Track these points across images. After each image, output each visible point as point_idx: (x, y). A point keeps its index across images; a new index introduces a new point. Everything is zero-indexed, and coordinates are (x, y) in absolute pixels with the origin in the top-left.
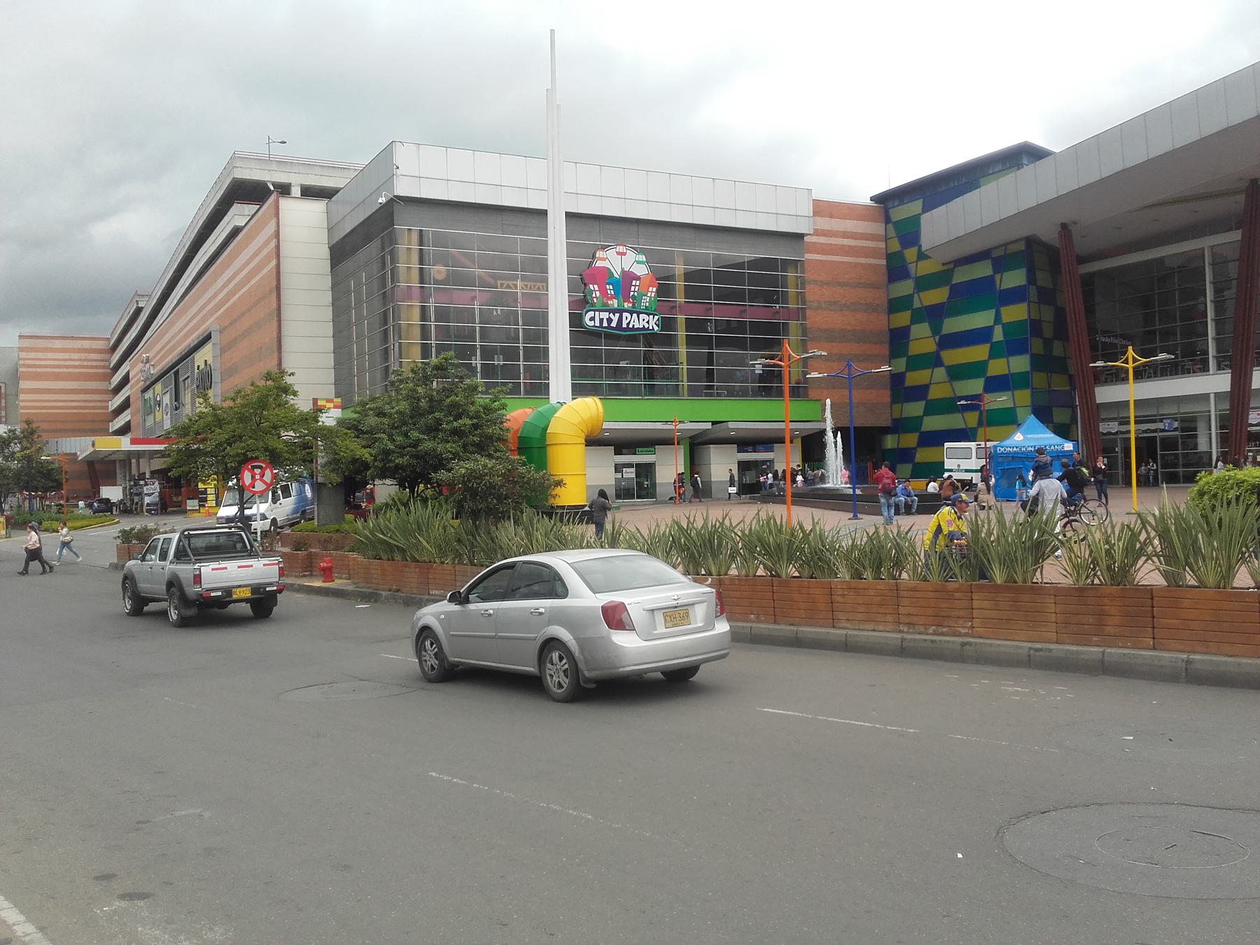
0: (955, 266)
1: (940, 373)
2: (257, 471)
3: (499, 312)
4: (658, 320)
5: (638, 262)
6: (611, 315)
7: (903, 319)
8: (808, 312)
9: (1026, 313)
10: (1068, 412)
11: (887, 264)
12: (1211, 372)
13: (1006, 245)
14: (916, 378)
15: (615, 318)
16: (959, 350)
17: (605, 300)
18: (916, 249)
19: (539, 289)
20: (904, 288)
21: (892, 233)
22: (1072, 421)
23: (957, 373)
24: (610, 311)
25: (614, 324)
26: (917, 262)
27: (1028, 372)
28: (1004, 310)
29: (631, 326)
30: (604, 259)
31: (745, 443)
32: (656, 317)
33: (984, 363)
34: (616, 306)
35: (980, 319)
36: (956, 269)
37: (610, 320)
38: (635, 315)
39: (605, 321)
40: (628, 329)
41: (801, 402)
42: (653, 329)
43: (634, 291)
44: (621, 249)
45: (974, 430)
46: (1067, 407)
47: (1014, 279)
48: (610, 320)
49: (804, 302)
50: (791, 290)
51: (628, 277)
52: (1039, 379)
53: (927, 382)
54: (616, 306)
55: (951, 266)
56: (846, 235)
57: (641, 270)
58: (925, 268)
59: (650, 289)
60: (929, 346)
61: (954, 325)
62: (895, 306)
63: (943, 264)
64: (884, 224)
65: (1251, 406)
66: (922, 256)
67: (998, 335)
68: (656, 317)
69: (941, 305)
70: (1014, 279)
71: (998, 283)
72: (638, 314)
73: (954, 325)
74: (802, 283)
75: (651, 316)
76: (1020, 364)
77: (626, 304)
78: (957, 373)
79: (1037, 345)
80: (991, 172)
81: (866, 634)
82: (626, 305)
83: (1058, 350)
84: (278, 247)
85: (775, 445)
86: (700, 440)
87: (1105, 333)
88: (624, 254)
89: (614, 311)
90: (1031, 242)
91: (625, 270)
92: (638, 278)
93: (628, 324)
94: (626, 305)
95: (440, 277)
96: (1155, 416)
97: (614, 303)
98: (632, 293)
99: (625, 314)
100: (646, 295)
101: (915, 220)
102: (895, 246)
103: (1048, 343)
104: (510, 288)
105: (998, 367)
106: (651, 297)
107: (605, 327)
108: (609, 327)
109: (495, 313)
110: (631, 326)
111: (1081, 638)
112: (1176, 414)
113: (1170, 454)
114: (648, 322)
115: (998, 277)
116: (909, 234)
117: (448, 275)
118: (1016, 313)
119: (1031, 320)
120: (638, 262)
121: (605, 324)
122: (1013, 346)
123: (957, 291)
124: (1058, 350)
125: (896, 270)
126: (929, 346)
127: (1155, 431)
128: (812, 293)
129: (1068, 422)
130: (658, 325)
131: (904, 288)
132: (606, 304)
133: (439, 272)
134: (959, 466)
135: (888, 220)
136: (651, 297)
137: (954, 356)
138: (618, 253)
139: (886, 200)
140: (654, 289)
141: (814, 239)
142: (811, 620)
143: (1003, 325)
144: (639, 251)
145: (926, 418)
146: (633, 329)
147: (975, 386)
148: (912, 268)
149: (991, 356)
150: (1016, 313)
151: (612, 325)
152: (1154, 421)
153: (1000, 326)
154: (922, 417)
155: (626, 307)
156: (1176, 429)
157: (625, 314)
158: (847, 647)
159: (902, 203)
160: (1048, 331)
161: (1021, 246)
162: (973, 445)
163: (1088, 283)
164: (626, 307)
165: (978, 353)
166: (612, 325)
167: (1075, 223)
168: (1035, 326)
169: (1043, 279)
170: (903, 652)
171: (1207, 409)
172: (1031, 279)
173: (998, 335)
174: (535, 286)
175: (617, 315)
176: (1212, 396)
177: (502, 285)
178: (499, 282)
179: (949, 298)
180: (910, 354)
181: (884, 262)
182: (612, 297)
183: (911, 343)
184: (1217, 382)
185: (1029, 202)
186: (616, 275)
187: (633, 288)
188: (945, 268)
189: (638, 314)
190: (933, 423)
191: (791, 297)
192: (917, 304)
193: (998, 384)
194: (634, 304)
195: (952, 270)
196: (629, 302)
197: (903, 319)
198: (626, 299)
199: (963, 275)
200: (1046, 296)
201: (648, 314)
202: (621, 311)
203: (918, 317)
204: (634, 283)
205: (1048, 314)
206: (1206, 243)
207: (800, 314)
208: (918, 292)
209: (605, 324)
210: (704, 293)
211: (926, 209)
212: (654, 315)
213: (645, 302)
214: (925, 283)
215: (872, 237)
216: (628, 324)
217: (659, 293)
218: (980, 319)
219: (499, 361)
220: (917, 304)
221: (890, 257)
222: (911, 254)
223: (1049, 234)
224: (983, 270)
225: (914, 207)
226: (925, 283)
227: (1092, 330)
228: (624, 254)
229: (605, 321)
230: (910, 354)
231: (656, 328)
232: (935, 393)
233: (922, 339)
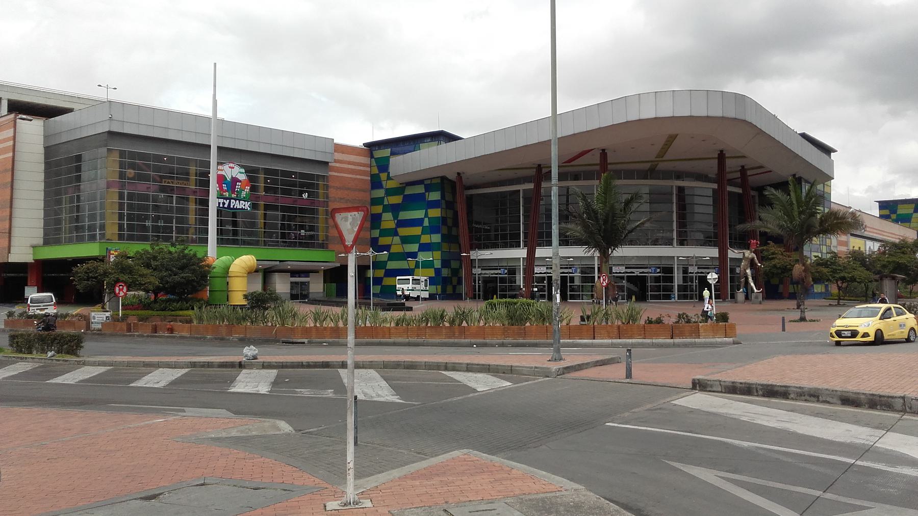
0: (407, 185)
1: (397, 239)
2: (121, 287)
3: (162, 196)
4: (250, 204)
5: (241, 173)
6: (225, 201)
7: (378, 209)
8: (330, 203)
9: (440, 213)
10: (458, 262)
11: (371, 180)
12: (521, 248)
13: (431, 179)
14: (383, 241)
15: (227, 202)
16: (405, 228)
17: (222, 193)
18: (386, 174)
19: (185, 185)
20: (380, 193)
21: (374, 164)
22: (460, 267)
23: (405, 240)
24: (224, 198)
25: (226, 206)
26: (386, 181)
27: (440, 243)
28: (429, 211)
29: (235, 207)
30: (222, 170)
31: (294, 273)
32: (249, 203)
33: (419, 237)
34: (227, 196)
35: (418, 214)
36: (407, 187)
37: (224, 204)
38: (237, 201)
39: (221, 204)
40: (233, 209)
41: (321, 252)
42: (247, 209)
43: (238, 188)
44: (231, 165)
45: (413, 270)
46: (458, 260)
47: (435, 196)
48: (224, 204)
49: (327, 197)
50: (321, 191)
51: (235, 180)
52: (445, 247)
53: (390, 243)
54: (227, 196)
55: (404, 185)
56: (349, 163)
57: (243, 177)
58: (391, 184)
59: (247, 188)
60: (392, 225)
61: (405, 215)
62: (375, 202)
63: (400, 184)
64: (370, 159)
65: (740, 179)
66: (389, 178)
67: (426, 223)
68: (249, 203)
69: (398, 205)
70: (435, 196)
71: (427, 198)
72: (239, 200)
73: (405, 215)
74: (327, 187)
75: (246, 202)
76: (436, 238)
77: (233, 195)
78: (405, 240)
79: (444, 230)
80: (425, 141)
81: (400, 340)
82: (233, 196)
83: (454, 232)
84: (14, 145)
85: (310, 274)
86: (272, 269)
87: (477, 223)
88: (233, 168)
89: (226, 199)
90: (443, 178)
91: (234, 176)
92: (240, 181)
93: (234, 206)
94: (233, 196)
95: (131, 176)
96: (497, 266)
97: (227, 194)
98: (236, 189)
99: (232, 200)
100: (244, 191)
101: (387, 158)
102: (375, 171)
103: (450, 228)
104: (170, 183)
105: (425, 239)
106: (246, 192)
107: (221, 207)
108: (223, 207)
109: (160, 197)
110: (235, 207)
111: (450, 338)
112: (506, 266)
113: (503, 286)
114: (244, 205)
115: (427, 194)
116: (383, 166)
117: (135, 175)
118: (435, 213)
119: (442, 217)
120: (241, 173)
121: (221, 206)
122: (433, 230)
123: (408, 199)
124: (454, 232)
125: (376, 183)
126: (392, 225)
127: (497, 274)
128: (332, 193)
129: (458, 268)
130: (250, 207)
131: (380, 193)
132: (222, 195)
133: (130, 173)
134: (408, 288)
135: (372, 157)
136: (246, 192)
137: (404, 231)
138: (230, 167)
139: (372, 147)
140: (249, 188)
141: (334, 164)
142: (383, 337)
143: (429, 218)
144: (242, 166)
145: (389, 262)
146: (237, 209)
147: (414, 248)
148: (384, 183)
149: (423, 233)
150: (435, 213)
151: (225, 206)
152: (497, 269)
153: (427, 219)
154: (387, 262)
155: (233, 196)
156: (506, 274)
157: (232, 200)
158: (394, 344)
159: (379, 149)
160: (450, 222)
161: (439, 181)
162: (410, 277)
163: (470, 198)
164: (233, 196)
165: (416, 231)
166: (225, 206)
167: (464, 173)
168: (444, 220)
169: (449, 197)
170: (409, 344)
171: (652, 196)
172: (443, 196)
173: (426, 223)
174: (178, 183)
175: (228, 201)
176: (522, 259)
177: (165, 182)
178: (164, 180)
179: (402, 202)
180: (381, 228)
181: (369, 178)
182: (226, 191)
183: (382, 222)
184: (521, 253)
185: (443, 161)
186: (228, 179)
187: (237, 187)
188: (401, 186)
189: (239, 200)
190: (392, 265)
191: (321, 195)
192: (386, 203)
193: (425, 247)
194: (237, 195)
195: (405, 187)
196: (235, 194)
197: (378, 209)
198: (233, 192)
199: (409, 191)
200: (450, 205)
201: (245, 201)
202: (230, 199)
203: (386, 209)
204: (238, 184)
205: (450, 214)
206: (521, 187)
207: (326, 204)
208: (386, 197)
209: (221, 206)
210: (275, 190)
211: (393, 154)
212: (248, 202)
213: (243, 194)
214: (390, 192)
215: (364, 165)
216: (234, 206)
217: (251, 190)
218: (418, 214)
219: (161, 224)
220: (386, 203)
221: (372, 176)
222: (383, 176)
223: (452, 176)
224: (420, 189)
225: (386, 152)
226: (390, 192)
227: (470, 222)
228: (233, 168)
229: (221, 204)
230: (381, 228)
231: (249, 209)
232: (394, 249)
233: (388, 222)
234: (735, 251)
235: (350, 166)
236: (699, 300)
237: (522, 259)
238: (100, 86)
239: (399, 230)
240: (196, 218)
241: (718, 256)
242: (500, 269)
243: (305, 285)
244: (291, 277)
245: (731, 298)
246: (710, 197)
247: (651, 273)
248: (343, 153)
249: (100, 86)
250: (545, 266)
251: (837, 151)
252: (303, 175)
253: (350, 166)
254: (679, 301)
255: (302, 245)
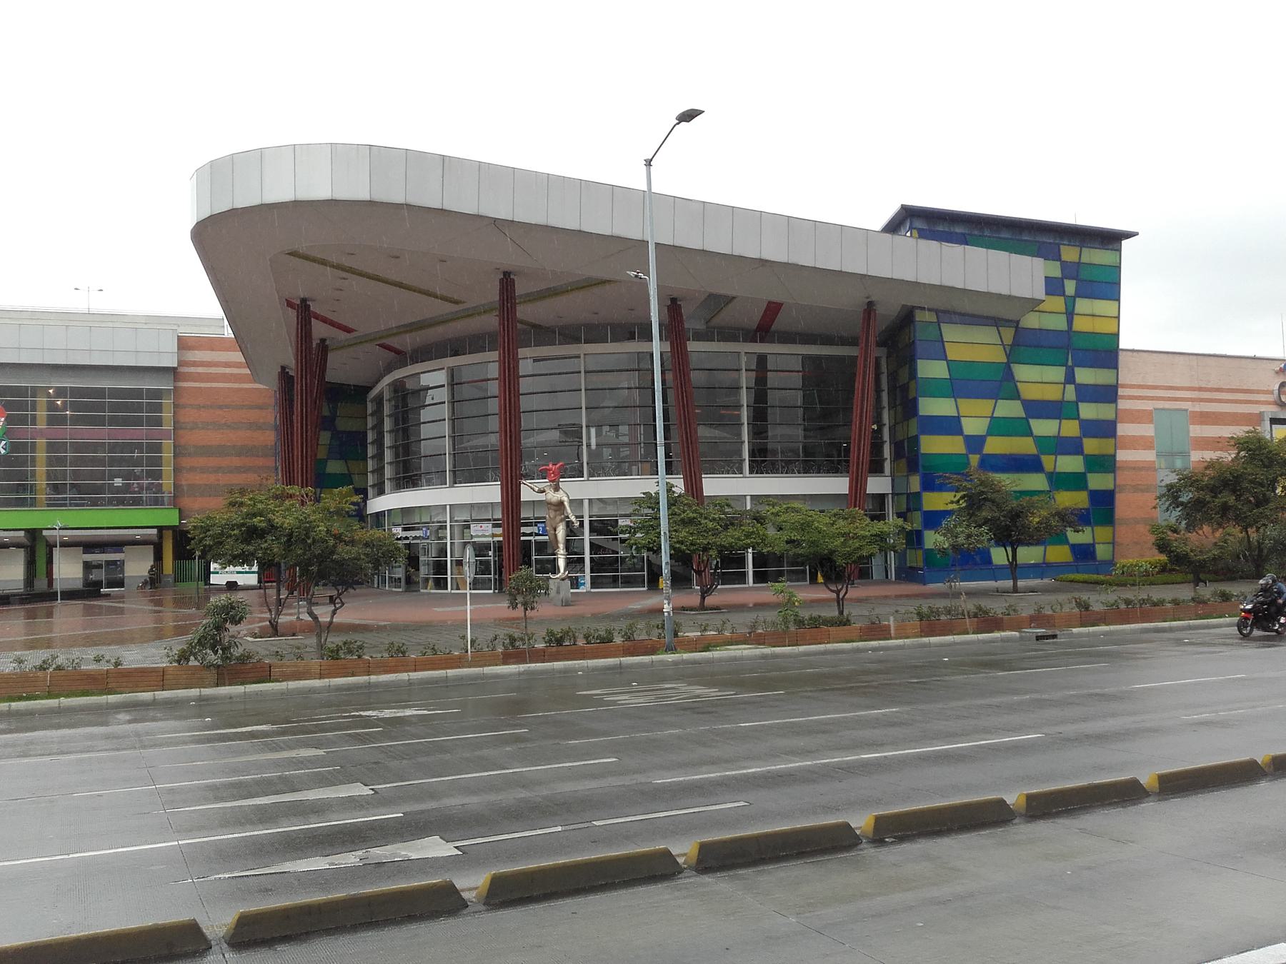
4: (5, 444)
31: (90, 546)
234: (1210, 455)
235: (228, 370)
236: (810, 583)
237: (448, 507)
238: (76, 289)
239: (1033, 422)
240: (669, 421)
241: (500, 501)
242: (536, 524)
243: (117, 566)
244: (84, 553)
245: (61, 599)
246: (694, 370)
247: (537, 535)
248: (213, 350)
249: (76, 289)
250: (489, 520)
251: (1137, 234)
252: (115, 393)
253: (228, 370)
254: (592, 590)
255: (121, 502)
